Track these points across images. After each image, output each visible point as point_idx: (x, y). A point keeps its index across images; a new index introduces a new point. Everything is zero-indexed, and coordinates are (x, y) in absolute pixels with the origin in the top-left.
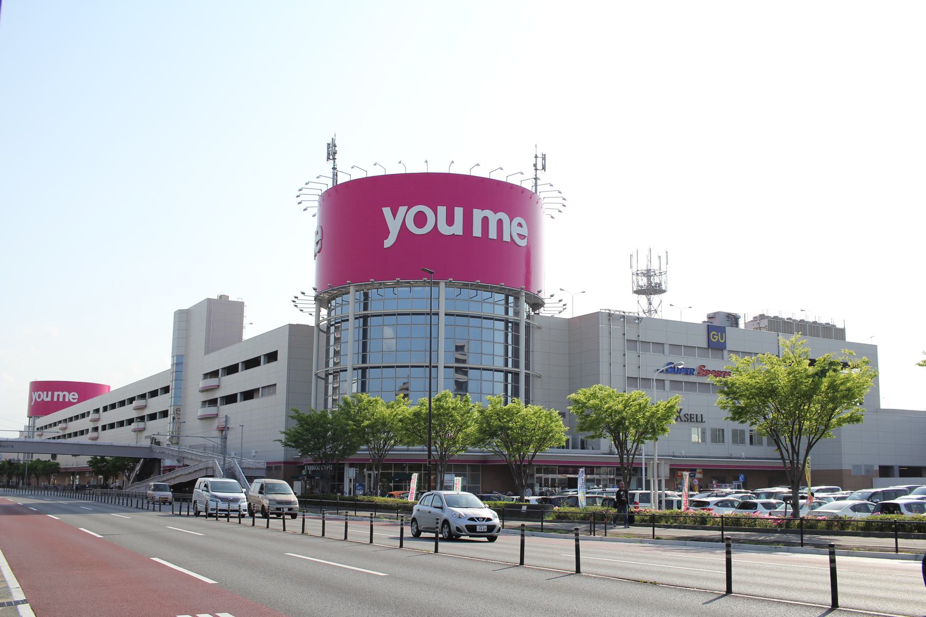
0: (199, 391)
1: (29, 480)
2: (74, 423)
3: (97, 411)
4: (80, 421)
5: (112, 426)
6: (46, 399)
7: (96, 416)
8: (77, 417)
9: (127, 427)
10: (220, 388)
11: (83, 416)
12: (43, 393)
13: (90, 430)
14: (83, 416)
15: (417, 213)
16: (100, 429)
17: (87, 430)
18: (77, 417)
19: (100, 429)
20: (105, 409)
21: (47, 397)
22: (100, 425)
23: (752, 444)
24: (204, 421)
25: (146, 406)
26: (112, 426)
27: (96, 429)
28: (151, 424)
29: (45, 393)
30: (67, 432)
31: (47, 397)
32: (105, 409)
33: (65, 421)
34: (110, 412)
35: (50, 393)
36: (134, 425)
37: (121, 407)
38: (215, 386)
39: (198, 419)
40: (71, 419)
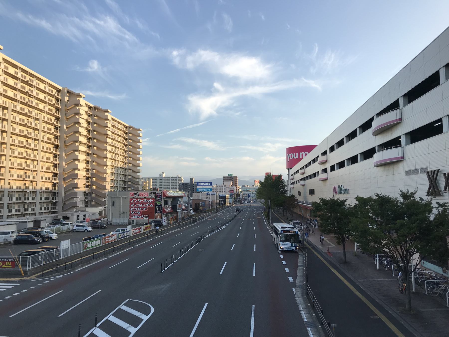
0: (373, 135)
1: (286, 227)
2: (309, 168)
3: (325, 153)
4: (313, 165)
5: (341, 165)
6: (295, 158)
7: (324, 158)
8: (310, 163)
9: (349, 167)
10: (328, 162)
11: (314, 161)
12: (293, 154)
13: (320, 172)
14: (314, 161)
15: (151, 309)
16: (329, 170)
17: (318, 172)
18: (310, 163)
19: (329, 170)
20: (332, 149)
21: (296, 156)
22: (328, 166)
23: (80, 162)
24: (379, 168)
25: (401, 120)
26: (341, 165)
27: (325, 171)
28: (309, 181)
29: (294, 154)
30: (305, 175)
31: (296, 156)
32: (332, 149)
33: (303, 167)
34: (338, 151)
35: (297, 154)
36: (378, 157)
37: (349, 140)
38: (396, 120)
39: (375, 166)
40: (306, 166)
